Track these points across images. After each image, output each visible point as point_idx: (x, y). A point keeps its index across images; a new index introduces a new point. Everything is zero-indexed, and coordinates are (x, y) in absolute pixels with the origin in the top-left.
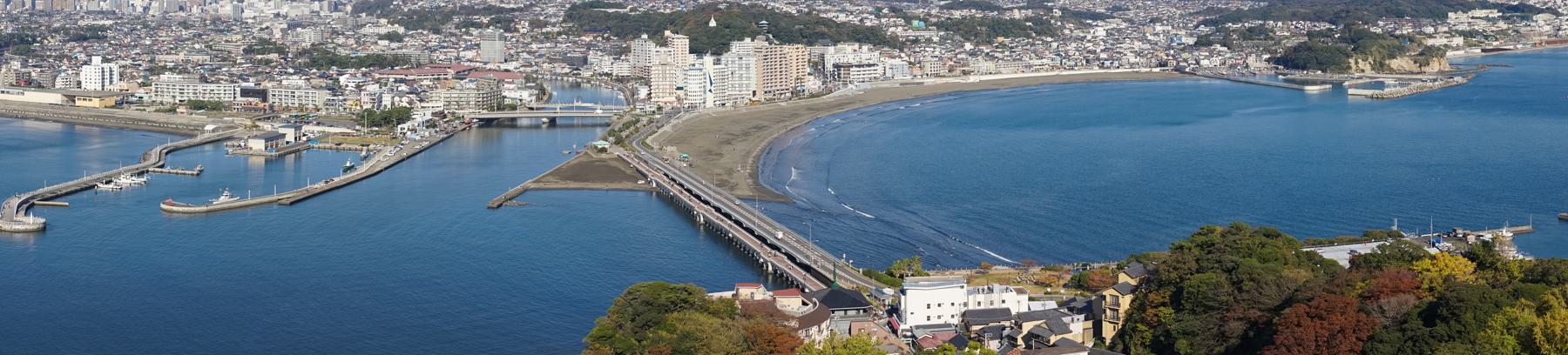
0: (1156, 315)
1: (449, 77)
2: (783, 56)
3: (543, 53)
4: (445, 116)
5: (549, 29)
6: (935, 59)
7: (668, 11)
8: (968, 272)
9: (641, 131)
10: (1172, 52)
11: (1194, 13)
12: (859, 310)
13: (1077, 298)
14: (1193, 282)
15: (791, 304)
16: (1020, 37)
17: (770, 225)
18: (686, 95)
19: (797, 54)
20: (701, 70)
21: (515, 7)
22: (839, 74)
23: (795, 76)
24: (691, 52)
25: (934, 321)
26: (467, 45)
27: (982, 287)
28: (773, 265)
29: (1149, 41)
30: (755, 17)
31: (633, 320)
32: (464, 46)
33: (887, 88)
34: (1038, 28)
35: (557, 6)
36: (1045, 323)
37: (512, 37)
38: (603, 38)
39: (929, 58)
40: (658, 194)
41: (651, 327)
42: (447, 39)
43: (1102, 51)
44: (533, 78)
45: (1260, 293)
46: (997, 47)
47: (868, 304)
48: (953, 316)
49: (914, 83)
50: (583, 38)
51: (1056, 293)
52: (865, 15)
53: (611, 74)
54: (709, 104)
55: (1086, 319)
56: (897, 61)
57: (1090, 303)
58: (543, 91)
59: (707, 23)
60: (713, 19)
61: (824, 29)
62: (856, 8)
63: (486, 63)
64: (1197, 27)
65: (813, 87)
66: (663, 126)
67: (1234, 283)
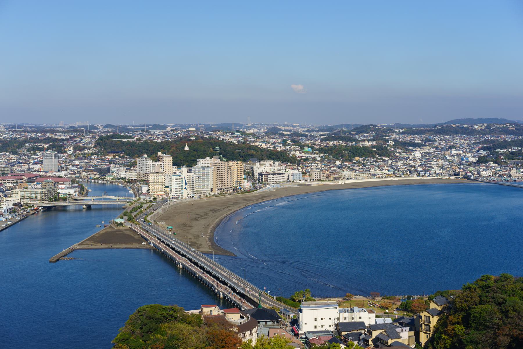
0: (453, 330)
1: (24, 181)
2: (229, 168)
3: (82, 166)
4: (22, 206)
5: (86, 151)
6: (318, 170)
7: (160, 141)
8: (340, 299)
9: (144, 212)
10: (462, 167)
11: (476, 143)
12: (274, 322)
13: (405, 317)
14: (477, 310)
15: (234, 317)
16: (369, 157)
17: (222, 270)
18: (171, 191)
20: (180, 176)
21: (64, 138)
22: (262, 179)
23: (236, 180)
24: (174, 165)
25: (319, 329)
26: (35, 162)
27: (347, 309)
28: (223, 294)
29: (448, 160)
30: (212, 144)
31: (141, 329)
32: (32, 162)
33: (291, 188)
34: (380, 152)
35: (90, 138)
36: (385, 331)
37: (63, 156)
38: (120, 157)
39: (315, 170)
40: (154, 250)
41: (152, 332)
42: (21, 158)
43: (419, 166)
44: (77, 181)
45: (520, 320)
46: (355, 163)
47: (279, 318)
48: (330, 326)
49: (305, 185)
50: (107, 157)
51: (391, 313)
52: (277, 144)
53: (125, 178)
54: (185, 196)
55: (410, 330)
56: (296, 171)
57: (413, 320)
58: (83, 189)
59: (183, 148)
60: (187, 146)
61: (253, 152)
62: (272, 140)
63: (46, 172)
64: (478, 151)
65: (247, 186)
66: (157, 209)
67: (502, 312)
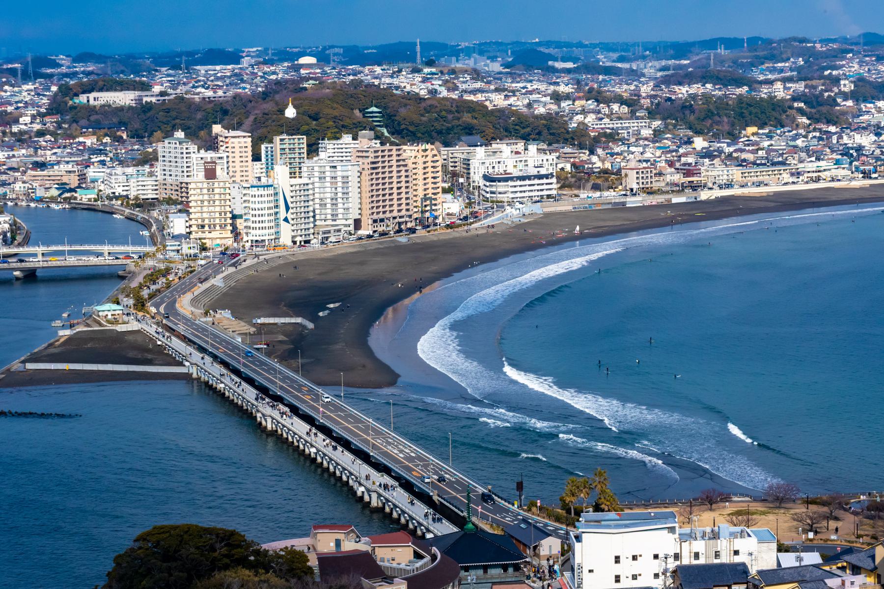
6: (645, 165)
19: (424, 159)
23: (421, 193)
52: (534, 97)
53: (127, 197)
59: (282, 112)
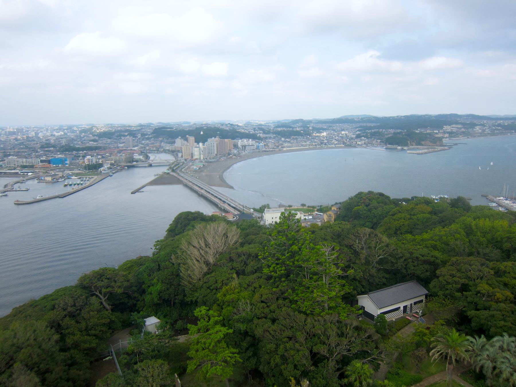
23: (229, 149)
37: (136, 139)
63: (127, 148)
